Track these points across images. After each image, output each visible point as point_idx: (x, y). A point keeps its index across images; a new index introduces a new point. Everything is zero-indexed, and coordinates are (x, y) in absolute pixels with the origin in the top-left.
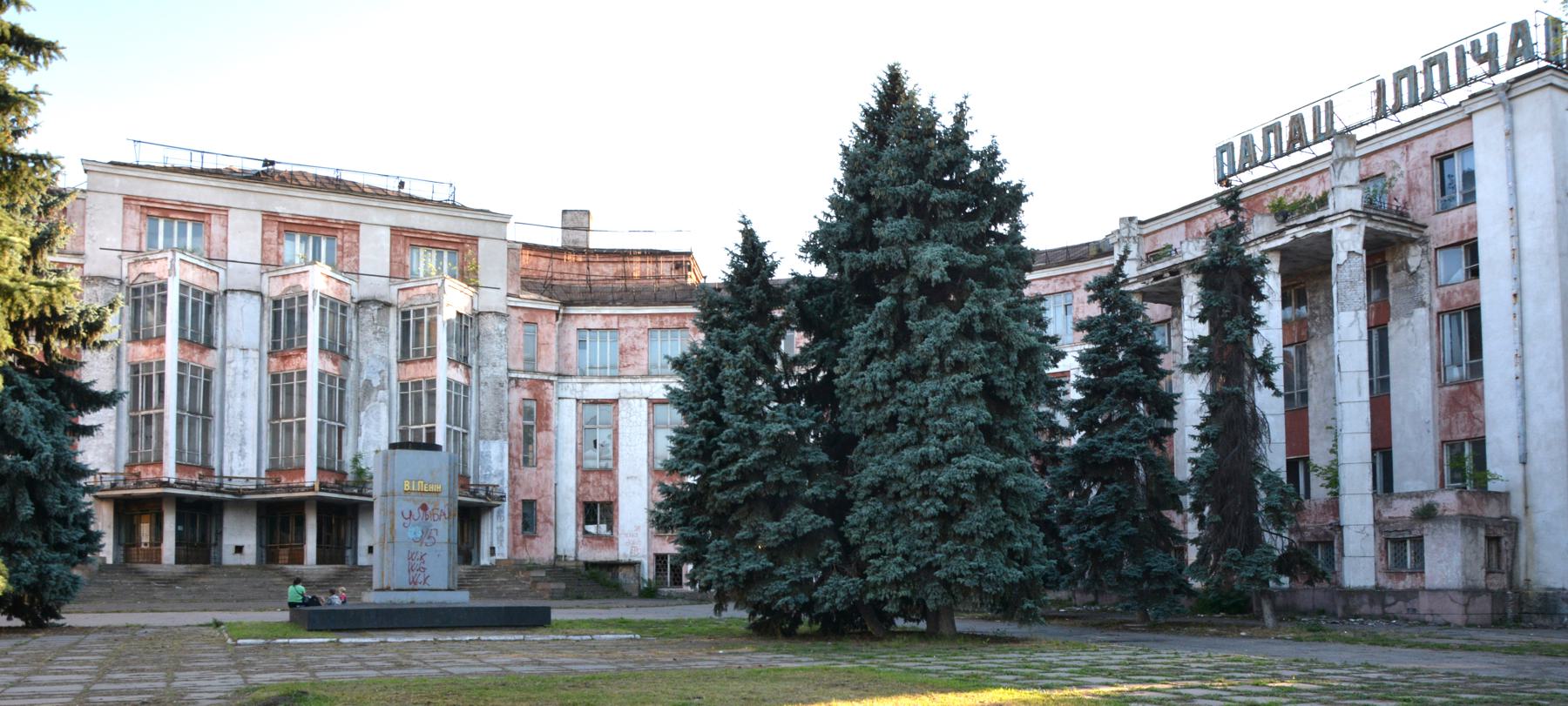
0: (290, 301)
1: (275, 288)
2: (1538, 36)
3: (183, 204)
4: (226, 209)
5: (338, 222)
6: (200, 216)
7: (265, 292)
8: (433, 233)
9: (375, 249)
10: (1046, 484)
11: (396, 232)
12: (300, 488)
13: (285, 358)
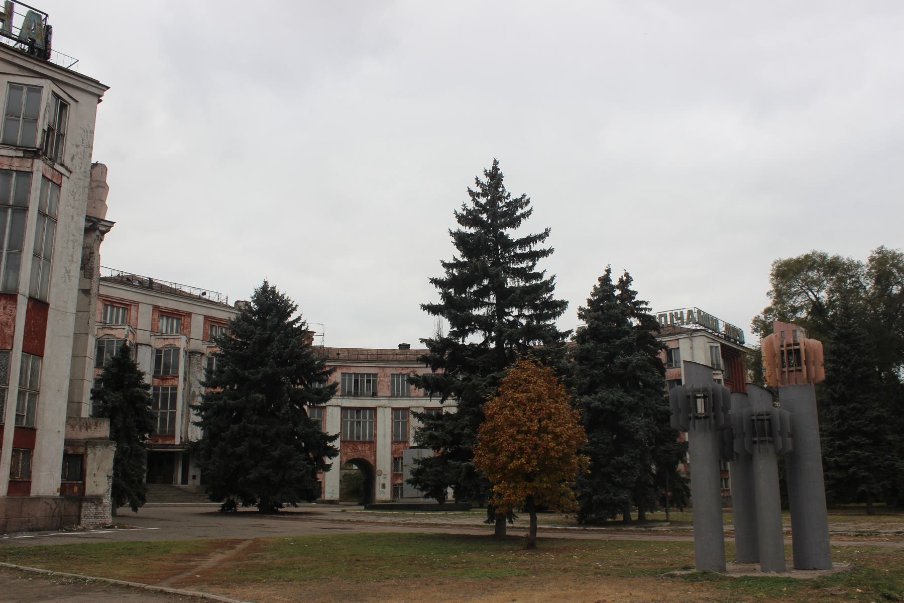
0: (168, 353)
1: (159, 344)
2: (696, 315)
3: (122, 299)
4: (138, 303)
5: (183, 312)
6: (126, 306)
7: (153, 344)
8: (221, 319)
9: (144, 317)
10: (275, 453)
11: (206, 318)
12: (173, 446)
13: (164, 379)
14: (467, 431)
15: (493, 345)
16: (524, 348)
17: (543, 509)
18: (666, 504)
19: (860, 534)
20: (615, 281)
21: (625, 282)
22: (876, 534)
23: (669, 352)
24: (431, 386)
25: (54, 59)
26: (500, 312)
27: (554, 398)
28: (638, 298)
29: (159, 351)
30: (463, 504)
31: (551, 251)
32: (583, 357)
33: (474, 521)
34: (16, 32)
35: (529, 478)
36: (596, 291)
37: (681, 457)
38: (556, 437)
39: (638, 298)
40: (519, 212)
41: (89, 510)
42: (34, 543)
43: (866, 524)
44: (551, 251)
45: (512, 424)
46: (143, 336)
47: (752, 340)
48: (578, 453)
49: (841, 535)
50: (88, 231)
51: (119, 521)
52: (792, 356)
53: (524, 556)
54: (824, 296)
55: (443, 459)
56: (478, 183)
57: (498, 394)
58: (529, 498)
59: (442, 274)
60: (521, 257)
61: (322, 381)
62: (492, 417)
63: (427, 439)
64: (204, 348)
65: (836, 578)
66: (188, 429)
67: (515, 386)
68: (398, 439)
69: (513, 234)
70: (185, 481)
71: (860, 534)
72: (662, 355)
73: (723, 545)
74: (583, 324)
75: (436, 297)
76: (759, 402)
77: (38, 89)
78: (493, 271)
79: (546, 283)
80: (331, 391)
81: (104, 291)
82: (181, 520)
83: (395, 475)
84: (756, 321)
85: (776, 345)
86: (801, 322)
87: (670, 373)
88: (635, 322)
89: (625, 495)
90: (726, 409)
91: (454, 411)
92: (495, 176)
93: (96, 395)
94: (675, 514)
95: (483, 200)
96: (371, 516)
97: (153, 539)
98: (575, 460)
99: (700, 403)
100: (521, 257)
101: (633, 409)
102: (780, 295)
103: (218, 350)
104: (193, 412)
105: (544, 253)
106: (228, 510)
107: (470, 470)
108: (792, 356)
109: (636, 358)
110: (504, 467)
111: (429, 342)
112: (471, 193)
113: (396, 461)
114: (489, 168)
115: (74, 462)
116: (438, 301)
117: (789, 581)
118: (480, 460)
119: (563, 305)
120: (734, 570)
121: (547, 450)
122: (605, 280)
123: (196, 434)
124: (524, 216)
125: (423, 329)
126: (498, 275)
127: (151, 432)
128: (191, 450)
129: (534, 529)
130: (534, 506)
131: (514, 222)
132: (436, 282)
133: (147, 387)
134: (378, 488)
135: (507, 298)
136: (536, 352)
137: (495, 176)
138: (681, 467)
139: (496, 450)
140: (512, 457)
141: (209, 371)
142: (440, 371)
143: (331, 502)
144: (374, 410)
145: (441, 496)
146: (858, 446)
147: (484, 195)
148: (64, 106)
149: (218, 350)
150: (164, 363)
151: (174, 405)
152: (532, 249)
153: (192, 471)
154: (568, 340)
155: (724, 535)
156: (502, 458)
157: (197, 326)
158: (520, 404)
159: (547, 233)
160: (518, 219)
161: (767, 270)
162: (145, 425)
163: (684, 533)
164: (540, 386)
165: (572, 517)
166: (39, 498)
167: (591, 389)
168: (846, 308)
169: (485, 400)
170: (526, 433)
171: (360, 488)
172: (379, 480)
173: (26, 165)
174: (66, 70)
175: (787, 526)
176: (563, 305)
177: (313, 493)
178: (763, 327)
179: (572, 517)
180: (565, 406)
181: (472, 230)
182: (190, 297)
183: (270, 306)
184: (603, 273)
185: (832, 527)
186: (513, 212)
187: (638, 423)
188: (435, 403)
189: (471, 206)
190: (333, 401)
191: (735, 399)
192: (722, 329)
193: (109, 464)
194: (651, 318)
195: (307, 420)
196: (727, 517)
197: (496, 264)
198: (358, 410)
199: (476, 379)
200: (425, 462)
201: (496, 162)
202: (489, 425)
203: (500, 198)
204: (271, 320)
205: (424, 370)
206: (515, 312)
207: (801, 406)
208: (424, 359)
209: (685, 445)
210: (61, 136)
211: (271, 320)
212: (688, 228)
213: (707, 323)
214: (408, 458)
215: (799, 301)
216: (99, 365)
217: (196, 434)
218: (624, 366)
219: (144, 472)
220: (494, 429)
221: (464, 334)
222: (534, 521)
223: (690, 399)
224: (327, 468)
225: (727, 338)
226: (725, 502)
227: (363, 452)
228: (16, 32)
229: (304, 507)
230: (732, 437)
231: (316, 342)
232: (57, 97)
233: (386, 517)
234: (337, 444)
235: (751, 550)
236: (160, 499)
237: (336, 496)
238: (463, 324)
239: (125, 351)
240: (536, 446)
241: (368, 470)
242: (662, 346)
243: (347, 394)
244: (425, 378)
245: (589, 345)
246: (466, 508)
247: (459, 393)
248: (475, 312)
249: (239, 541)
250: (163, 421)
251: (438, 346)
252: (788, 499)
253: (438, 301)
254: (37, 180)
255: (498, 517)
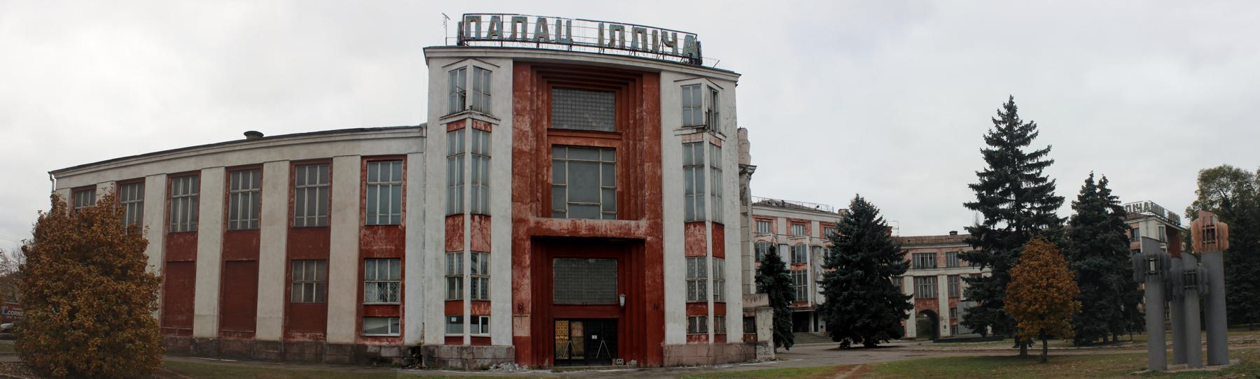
1: (793, 243)
6: (769, 220)
9: (781, 226)
11: (821, 223)
14: (999, 288)
15: (1014, 229)
16: (1035, 231)
17: (1051, 337)
18: (1130, 330)
19: (1246, 342)
20: (1096, 183)
21: (1103, 183)
22: (1254, 341)
23: (1132, 231)
24: (973, 259)
25: (704, 64)
26: (1018, 206)
27: (1057, 264)
28: (1112, 194)
29: (793, 248)
30: (997, 337)
31: (1052, 161)
32: (1076, 235)
33: (1006, 347)
34: (680, 52)
35: (1041, 317)
36: (1084, 190)
37: (1140, 300)
38: (1059, 289)
39: (1112, 194)
40: (1029, 134)
41: (760, 350)
42: (732, 370)
43: (1249, 336)
44: (1052, 161)
45: (1029, 282)
46: (782, 239)
47: (1185, 223)
48: (1073, 300)
49: (1234, 343)
50: (741, 174)
51: (779, 356)
52: (1209, 233)
53: (1040, 368)
54: (1229, 194)
55: (984, 307)
56: (999, 113)
57: (1019, 263)
58: (1042, 330)
59: (977, 181)
60: (1032, 167)
61: (899, 260)
62: (1015, 278)
63: (972, 295)
64: (821, 243)
65: (1231, 369)
66: (816, 296)
67: (1031, 256)
68: (953, 296)
69: (1025, 150)
70: (816, 330)
71: (1246, 342)
72: (1128, 233)
73: (1165, 354)
74: (1075, 212)
75: (973, 197)
76: (1189, 263)
77: (698, 86)
78: (1012, 177)
79: (1049, 185)
80: (906, 266)
81: (755, 212)
82: (816, 353)
83: (953, 319)
84: (1188, 210)
85: (1200, 225)
86: (1215, 211)
87: (1133, 245)
88: (1110, 211)
89: (1104, 326)
90: (1168, 268)
91: (989, 275)
92: (1011, 108)
93: (758, 279)
94: (1136, 336)
95: (1003, 126)
96: (938, 347)
97: (800, 366)
98: (1071, 304)
99: (1152, 264)
100: (1032, 167)
101: (1109, 269)
102: (1203, 193)
103: (830, 244)
104: (818, 286)
105: (1047, 163)
106: (845, 347)
107: (1002, 314)
108: (1209, 233)
109: (1111, 235)
110: (1025, 311)
111: (970, 229)
112: (995, 121)
113: (953, 310)
114: (1007, 102)
115: (749, 322)
116: (975, 200)
117: (1205, 373)
118: (1009, 307)
119: (1061, 199)
120: (1172, 368)
121: (1053, 299)
122: (1089, 182)
123: (821, 300)
124: (1032, 136)
125: (966, 220)
126: (1015, 180)
127: (793, 300)
128: (820, 310)
129: (1045, 350)
130: (1045, 336)
131: (1026, 142)
132: (973, 186)
133: (788, 272)
134: (941, 328)
135: (1023, 196)
136: (1043, 233)
137: (1011, 108)
138: (1140, 306)
139: (1019, 300)
140: (1030, 304)
141: (826, 258)
142: (979, 249)
143: (911, 339)
144: (935, 277)
145: (983, 332)
146: (1246, 289)
147: (1004, 122)
148: (715, 93)
149: (830, 244)
150: (797, 257)
151: (805, 282)
152: (1038, 161)
153: (820, 323)
154: (1065, 224)
155: (1166, 347)
156: (1023, 305)
157: (816, 229)
158: (1034, 268)
159: (1049, 149)
160: (1029, 139)
161: (1196, 176)
162: (789, 296)
163: (1142, 347)
164: (1047, 256)
165: (1070, 342)
166: (731, 344)
167: (1081, 257)
168: (1242, 203)
169: (1009, 267)
170: (1039, 287)
171: (929, 328)
172: (942, 324)
173: (698, 138)
174: (713, 69)
175: (1204, 340)
176: (1061, 199)
177: (898, 333)
178: (1192, 214)
179: (1070, 342)
180: (1064, 269)
181: (997, 148)
182: (809, 210)
183: (862, 212)
184: (1088, 177)
185: (1230, 339)
186: (1025, 134)
187: (1112, 278)
188: (976, 270)
189: (995, 130)
190: (908, 273)
191: (1174, 261)
192: (1166, 215)
193: (770, 322)
194: (1120, 208)
195: (892, 286)
196: (1168, 336)
197: (1014, 172)
198: (925, 277)
199: (1004, 253)
200: (972, 310)
201: (1011, 98)
202: (1014, 283)
203: (1016, 124)
204: (863, 221)
205: (968, 249)
206: (1029, 205)
207: (1214, 265)
208: (967, 241)
209: (1143, 292)
210: (717, 114)
211: (863, 221)
212: (1139, 152)
213: (1157, 211)
214: (961, 307)
215: (1215, 197)
216: (757, 260)
217: (821, 300)
218: (1103, 241)
219: (791, 326)
220: (1017, 286)
221: (994, 222)
222: (1045, 345)
223: (1146, 262)
224: (907, 317)
225: (1170, 221)
226: (1167, 327)
227: (930, 305)
228: (680, 52)
229: (893, 343)
230: (1172, 286)
231: (894, 234)
232: (710, 88)
233: (948, 347)
234: (912, 301)
235: (1183, 355)
236: (801, 341)
237: (914, 335)
238: (993, 216)
239: (772, 249)
240: (1046, 296)
241: (934, 317)
242: (1128, 227)
243: (917, 268)
244: (968, 253)
245: (1079, 227)
246: (1001, 339)
247: (992, 263)
248: (1001, 207)
249: (854, 366)
250: (800, 292)
251: (976, 232)
252: (1205, 324)
253: (975, 200)
254: (706, 145)
255: (1022, 343)
